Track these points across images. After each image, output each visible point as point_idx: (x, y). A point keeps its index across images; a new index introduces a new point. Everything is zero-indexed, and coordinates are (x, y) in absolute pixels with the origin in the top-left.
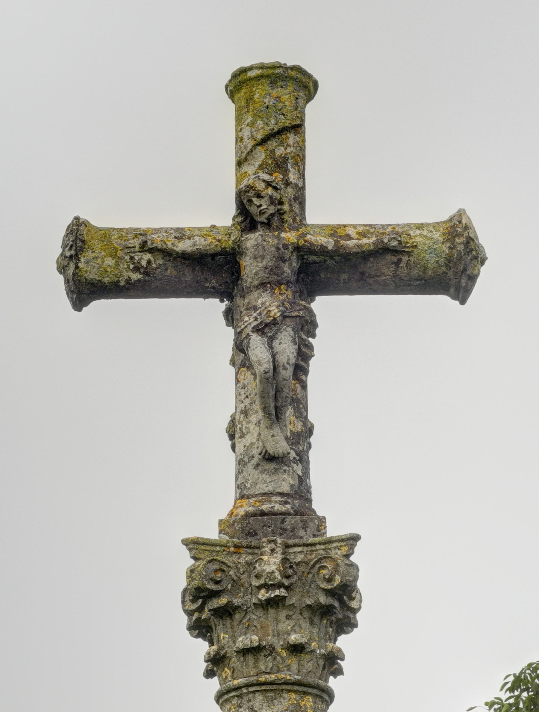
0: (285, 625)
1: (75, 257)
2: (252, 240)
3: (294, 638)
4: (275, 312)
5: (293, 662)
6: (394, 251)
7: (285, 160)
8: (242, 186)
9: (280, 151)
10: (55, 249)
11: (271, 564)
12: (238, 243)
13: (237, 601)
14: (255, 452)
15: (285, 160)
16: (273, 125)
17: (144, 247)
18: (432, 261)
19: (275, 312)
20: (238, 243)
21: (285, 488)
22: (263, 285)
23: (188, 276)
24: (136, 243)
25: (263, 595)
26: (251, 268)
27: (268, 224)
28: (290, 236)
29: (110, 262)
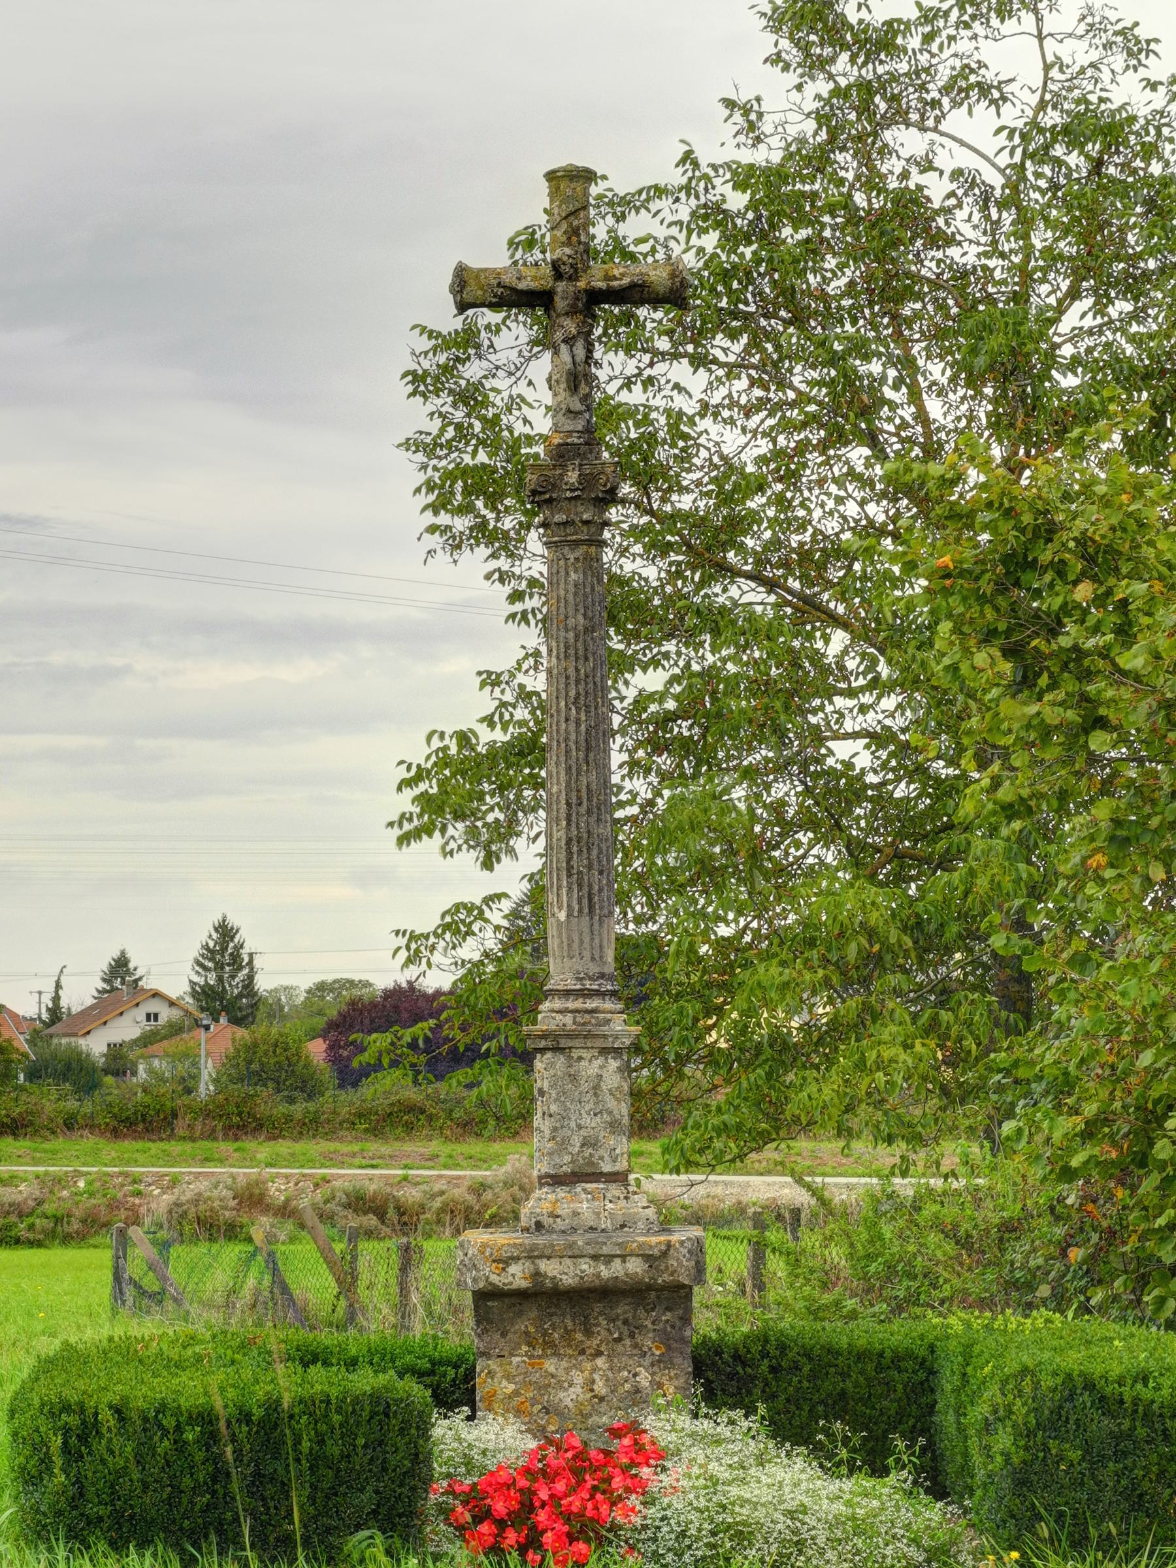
0: (581, 509)
1: (461, 292)
2: (561, 286)
3: (585, 517)
4: (574, 331)
5: (585, 529)
6: (640, 286)
7: (578, 228)
8: (602, 1186)
9: (576, 223)
10: (448, 279)
11: (572, 477)
12: (553, 288)
13: (554, 495)
14: (564, 406)
15: (578, 228)
16: (571, 208)
17: (499, 285)
18: (661, 290)
19: (574, 331)
20: (553, 288)
21: (580, 428)
22: (567, 314)
23: (524, 300)
24: (495, 282)
25: (568, 494)
26: (560, 304)
27: (570, 279)
28: (582, 284)
29: (480, 292)
